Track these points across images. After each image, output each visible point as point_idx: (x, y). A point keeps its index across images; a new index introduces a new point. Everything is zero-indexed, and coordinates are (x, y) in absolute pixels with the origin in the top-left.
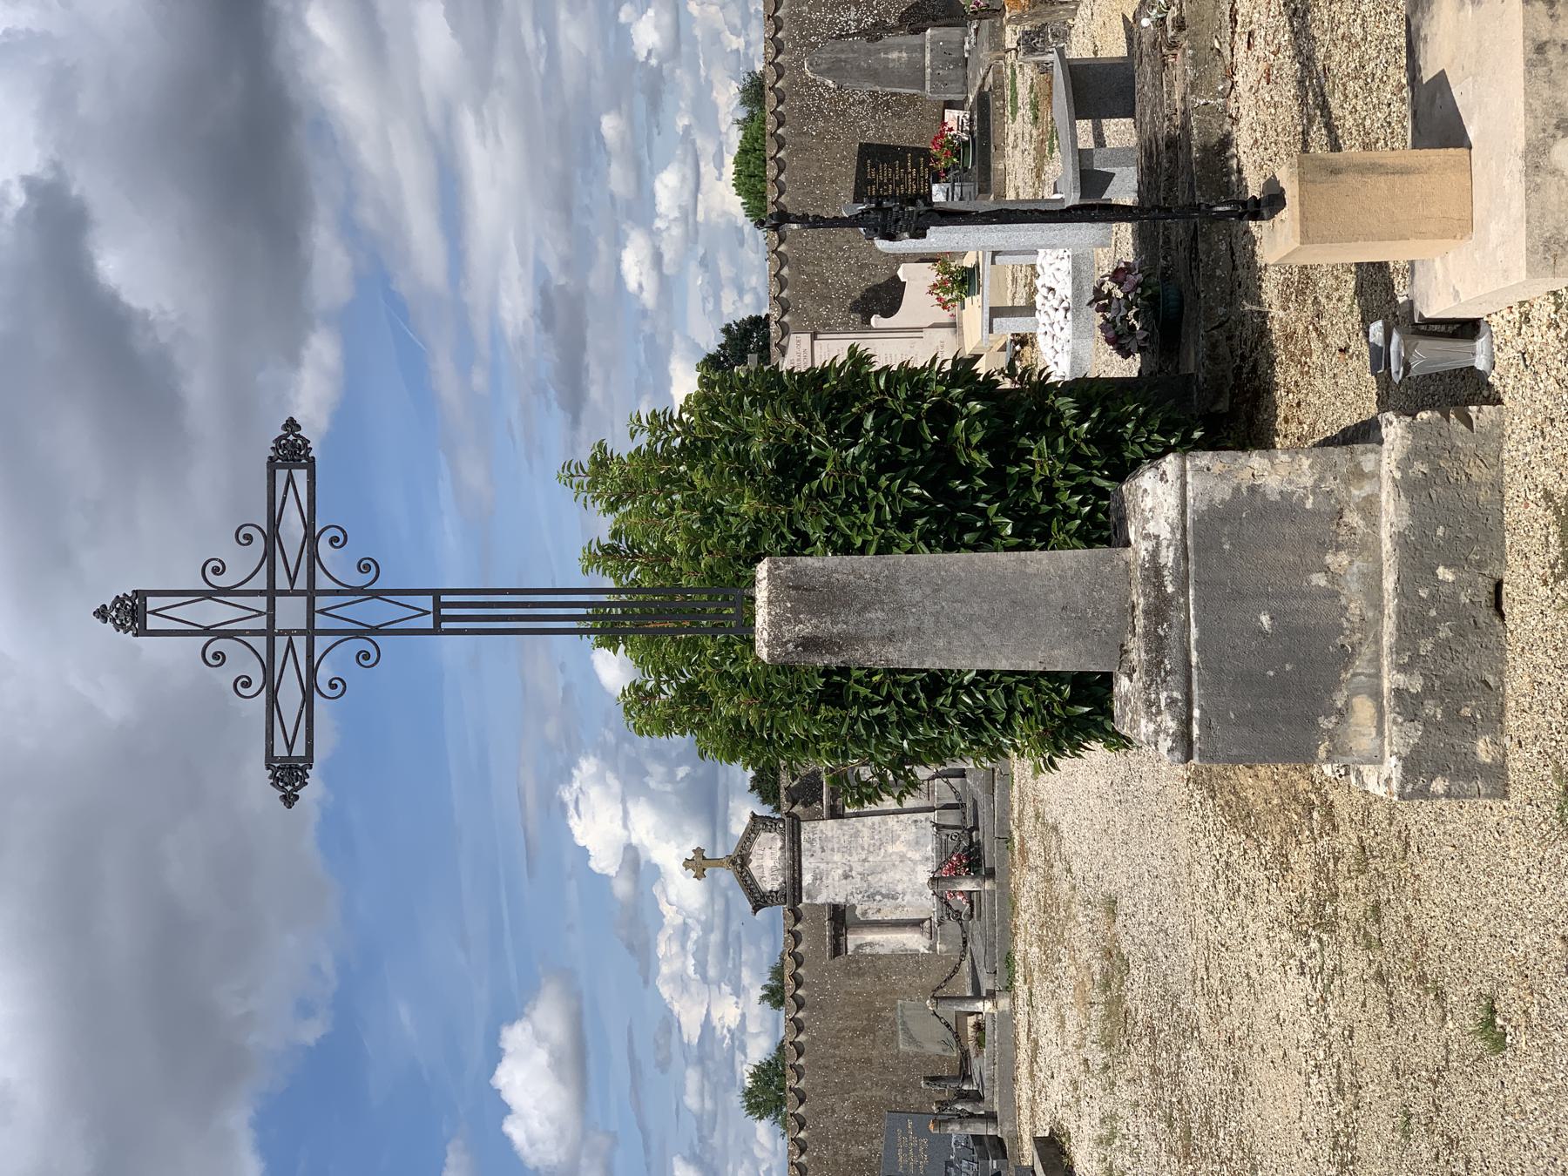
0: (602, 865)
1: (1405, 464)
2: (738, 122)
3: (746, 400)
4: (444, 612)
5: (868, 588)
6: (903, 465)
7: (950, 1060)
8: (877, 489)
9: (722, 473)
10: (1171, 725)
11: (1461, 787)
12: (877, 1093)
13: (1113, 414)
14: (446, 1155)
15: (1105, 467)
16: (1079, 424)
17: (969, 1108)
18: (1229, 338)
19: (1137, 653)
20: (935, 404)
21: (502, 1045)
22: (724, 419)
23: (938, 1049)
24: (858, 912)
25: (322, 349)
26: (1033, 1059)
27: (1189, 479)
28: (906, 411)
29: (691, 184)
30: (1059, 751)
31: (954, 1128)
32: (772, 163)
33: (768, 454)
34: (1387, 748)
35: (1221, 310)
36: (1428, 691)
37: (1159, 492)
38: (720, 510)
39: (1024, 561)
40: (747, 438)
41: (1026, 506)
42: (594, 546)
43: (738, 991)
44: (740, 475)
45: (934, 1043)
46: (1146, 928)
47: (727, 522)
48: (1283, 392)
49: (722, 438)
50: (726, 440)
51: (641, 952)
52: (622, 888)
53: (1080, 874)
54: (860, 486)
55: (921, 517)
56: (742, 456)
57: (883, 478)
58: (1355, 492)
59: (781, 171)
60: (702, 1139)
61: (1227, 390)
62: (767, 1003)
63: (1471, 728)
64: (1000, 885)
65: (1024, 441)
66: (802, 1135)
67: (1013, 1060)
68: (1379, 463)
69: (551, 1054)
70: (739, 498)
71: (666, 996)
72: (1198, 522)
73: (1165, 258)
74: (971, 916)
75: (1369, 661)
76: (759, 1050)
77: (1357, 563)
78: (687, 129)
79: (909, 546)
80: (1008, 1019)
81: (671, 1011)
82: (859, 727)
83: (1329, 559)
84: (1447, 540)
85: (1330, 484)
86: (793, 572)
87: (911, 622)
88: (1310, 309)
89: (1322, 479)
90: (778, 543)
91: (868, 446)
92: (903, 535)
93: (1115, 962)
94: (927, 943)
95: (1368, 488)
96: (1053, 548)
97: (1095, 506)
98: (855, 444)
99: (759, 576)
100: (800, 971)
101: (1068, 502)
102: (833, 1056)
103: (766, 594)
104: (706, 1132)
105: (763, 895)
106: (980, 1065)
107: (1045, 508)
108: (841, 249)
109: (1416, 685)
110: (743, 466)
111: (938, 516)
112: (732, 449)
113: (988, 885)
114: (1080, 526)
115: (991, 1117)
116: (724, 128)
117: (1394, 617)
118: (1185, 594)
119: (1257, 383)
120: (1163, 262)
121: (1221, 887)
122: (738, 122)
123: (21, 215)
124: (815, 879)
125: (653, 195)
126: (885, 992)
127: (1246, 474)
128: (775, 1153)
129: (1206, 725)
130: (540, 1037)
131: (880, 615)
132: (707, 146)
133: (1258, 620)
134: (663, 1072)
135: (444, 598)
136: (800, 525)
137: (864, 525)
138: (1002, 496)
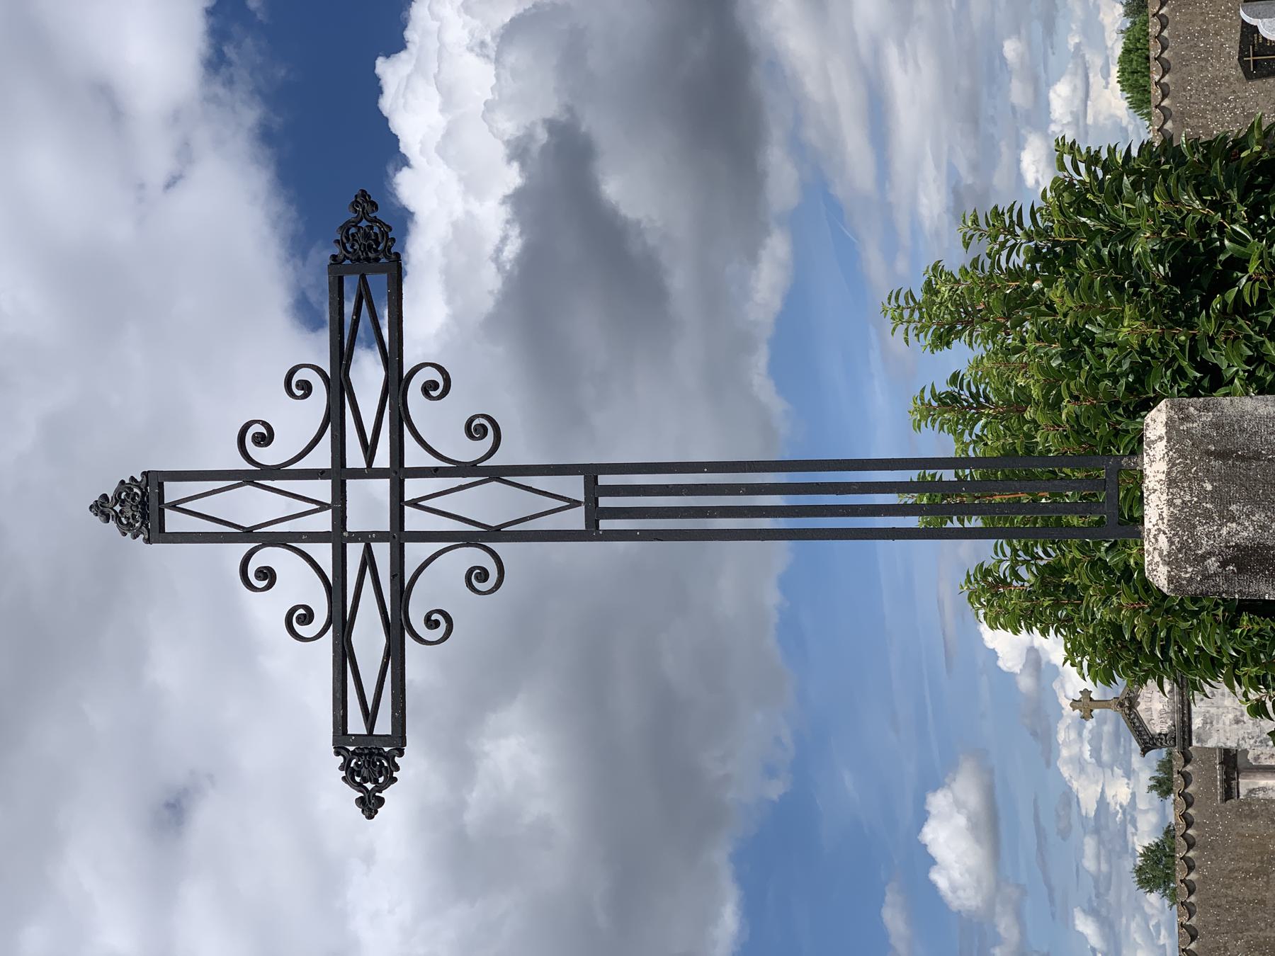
0: (1009, 664)
2: (1122, 32)
3: (1126, 181)
4: (604, 502)
9: (1091, 286)
14: (884, 894)
21: (927, 808)
22: (1095, 211)
24: (1250, 757)
25: (777, 247)
29: (1080, 94)
32: (1155, 20)
33: (1158, 257)
38: (1090, 340)
40: (1128, 235)
42: (927, 396)
43: (1129, 773)
44: (1119, 289)
47: (1101, 356)
49: (1090, 239)
50: (1098, 241)
51: (1044, 737)
52: (1026, 683)
56: (1121, 262)
59: (1163, 27)
60: (1098, 896)
62: (1155, 793)
69: (969, 819)
70: (1116, 320)
71: (1066, 775)
76: (1145, 836)
78: (1078, 46)
81: (1070, 788)
86: (1217, 426)
90: (1174, 381)
99: (1150, 434)
100: (1190, 811)
103: (1163, 466)
104: (1102, 890)
105: (1152, 738)
108: (1226, 100)
110: (1122, 277)
112: (1105, 252)
116: (1109, 44)
122: (1122, 32)
123: (544, 149)
124: (1205, 723)
125: (1048, 104)
128: (1162, 912)
130: (959, 805)
132: (1096, 61)
134: (1064, 839)
135: (604, 480)
136: (1210, 355)
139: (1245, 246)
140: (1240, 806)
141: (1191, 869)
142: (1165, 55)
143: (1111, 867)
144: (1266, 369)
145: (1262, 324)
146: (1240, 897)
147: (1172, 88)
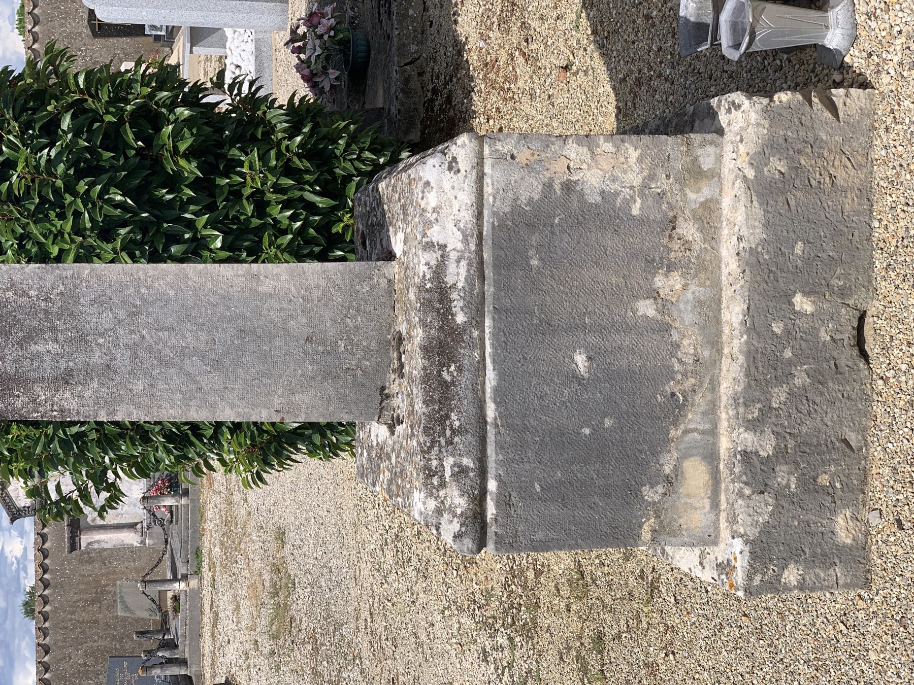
1: (759, 160)
5: (33, 310)
6: (106, 171)
7: (154, 621)
8: (75, 194)
10: (460, 502)
11: (817, 576)
12: (101, 643)
13: (324, 130)
15: (316, 182)
16: (290, 138)
17: (167, 654)
18: (420, 74)
19: (409, 398)
20: (140, 107)
23: (146, 615)
24: (89, 519)
26: (214, 626)
27: (487, 169)
28: (108, 112)
30: (267, 463)
31: (157, 672)
34: (723, 524)
35: (413, 48)
36: (781, 453)
37: (447, 186)
39: (256, 276)
41: (236, 219)
45: (143, 611)
46: (312, 561)
48: (483, 119)
53: (254, 506)
54: (56, 191)
55: (124, 225)
57: (82, 183)
58: (692, 196)
61: (418, 123)
63: (829, 500)
64: (193, 501)
65: (235, 152)
66: (47, 676)
67: (200, 622)
68: (719, 158)
72: (500, 227)
73: (352, 9)
74: (172, 522)
75: (704, 413)
77: (692, 288)
79: (111, 256)
80: (196, 594)
82: (55, 445)
83: (659, 281)
84: (808, 261)
85: (662, 184)
87: (97, 357)
88: (516, 36)
89: (652, 177)
91: (68, 148)
92: (104, 245)
93: (281, 584)
94: (139, 539)
95: (706, 191)
96: (263, 262)
97: (306, 220)
98: (51, 145)
100: (46, 561)
101: (279, 217)
102: (71, 620)
105: (19, 510)
106: (177, 624)
107: (256, 222)
108: (80, 50)
109: (767, 446)
111: (144, 226)
113: (184, 501)
114: (292, 240)
115: (183, 662)
117: (741, 359)
118: (480, 325)
119: (452, 113)
120: (351, 13)
121: (389, 554)
126: (108, 573)
127: (560, 166)
129: (504, 502)
131: (52, 347)
133: (572, 360)
137: (61, 233)
138: (211, 208)
139: (17, 152)
140: (81, 555)
141: (46, 603)
142: (36, 11)
143: (7, 603)
144: (33, 244)
145: (28, 210)
146: (81, 619)
147: (40, 36)
